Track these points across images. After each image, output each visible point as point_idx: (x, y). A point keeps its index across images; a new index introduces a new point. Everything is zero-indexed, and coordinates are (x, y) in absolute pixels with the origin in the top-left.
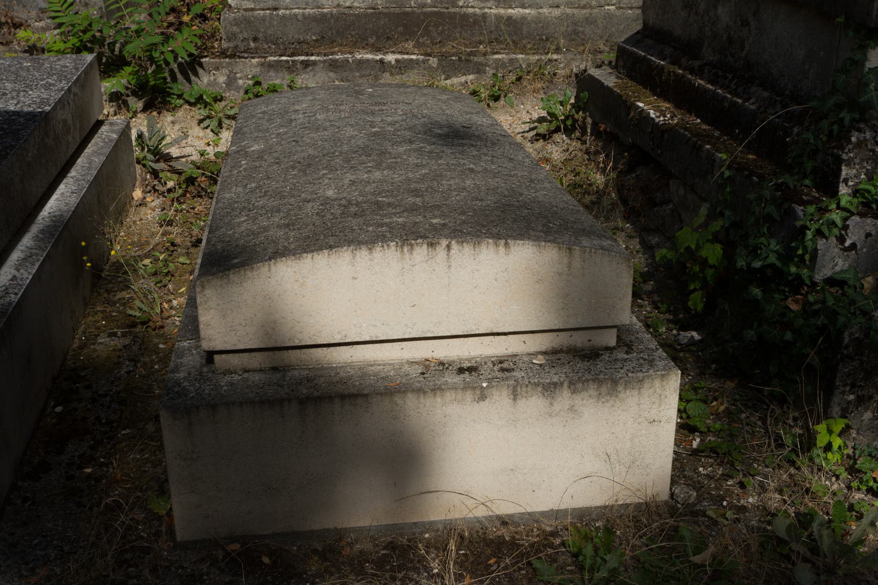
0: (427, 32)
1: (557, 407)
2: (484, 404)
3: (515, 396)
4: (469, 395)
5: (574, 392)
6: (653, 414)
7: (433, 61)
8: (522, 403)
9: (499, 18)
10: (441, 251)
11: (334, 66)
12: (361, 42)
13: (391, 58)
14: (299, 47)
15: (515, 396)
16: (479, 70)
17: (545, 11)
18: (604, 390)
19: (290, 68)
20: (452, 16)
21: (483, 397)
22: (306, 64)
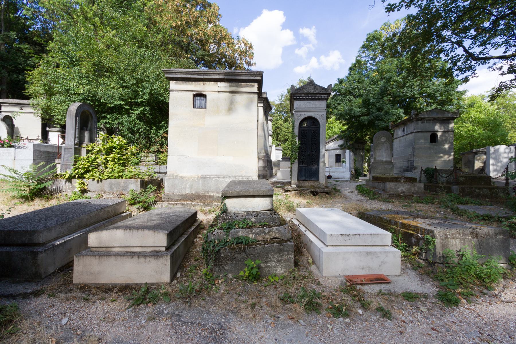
0: (202, 198)
1: (146, 260)
2: (133, 259)
3: (138, 258)
4: (130, 257)
5: (150, 258)
6: (165, 263)
7: (202, 204)
8: (140, 259)
9: (217, 196)
10: (131, 231)
11: (182, 204)
12: (188, 200)
13: (194, 203)
14: (177, 200)
15: (138, 258)
16: (211, 206)
17: (186, 203)
18: (155, 257)
19: (174, 204)
20: (207, 196)
21: (132, 258)
22: (177, 204)
